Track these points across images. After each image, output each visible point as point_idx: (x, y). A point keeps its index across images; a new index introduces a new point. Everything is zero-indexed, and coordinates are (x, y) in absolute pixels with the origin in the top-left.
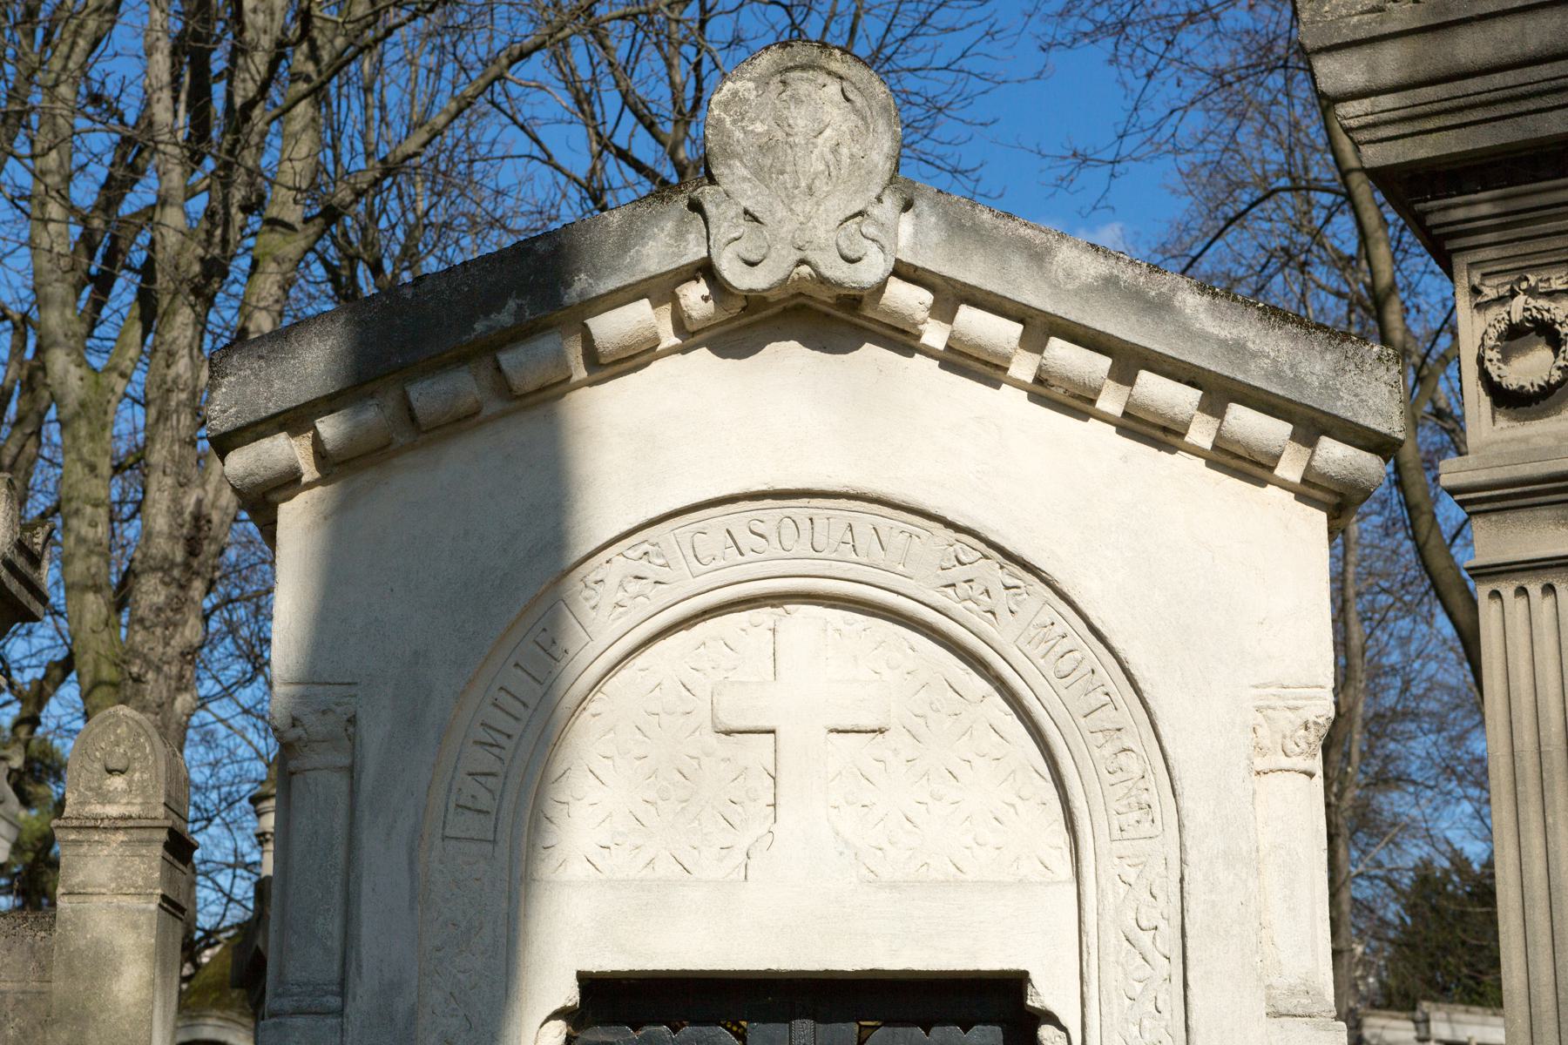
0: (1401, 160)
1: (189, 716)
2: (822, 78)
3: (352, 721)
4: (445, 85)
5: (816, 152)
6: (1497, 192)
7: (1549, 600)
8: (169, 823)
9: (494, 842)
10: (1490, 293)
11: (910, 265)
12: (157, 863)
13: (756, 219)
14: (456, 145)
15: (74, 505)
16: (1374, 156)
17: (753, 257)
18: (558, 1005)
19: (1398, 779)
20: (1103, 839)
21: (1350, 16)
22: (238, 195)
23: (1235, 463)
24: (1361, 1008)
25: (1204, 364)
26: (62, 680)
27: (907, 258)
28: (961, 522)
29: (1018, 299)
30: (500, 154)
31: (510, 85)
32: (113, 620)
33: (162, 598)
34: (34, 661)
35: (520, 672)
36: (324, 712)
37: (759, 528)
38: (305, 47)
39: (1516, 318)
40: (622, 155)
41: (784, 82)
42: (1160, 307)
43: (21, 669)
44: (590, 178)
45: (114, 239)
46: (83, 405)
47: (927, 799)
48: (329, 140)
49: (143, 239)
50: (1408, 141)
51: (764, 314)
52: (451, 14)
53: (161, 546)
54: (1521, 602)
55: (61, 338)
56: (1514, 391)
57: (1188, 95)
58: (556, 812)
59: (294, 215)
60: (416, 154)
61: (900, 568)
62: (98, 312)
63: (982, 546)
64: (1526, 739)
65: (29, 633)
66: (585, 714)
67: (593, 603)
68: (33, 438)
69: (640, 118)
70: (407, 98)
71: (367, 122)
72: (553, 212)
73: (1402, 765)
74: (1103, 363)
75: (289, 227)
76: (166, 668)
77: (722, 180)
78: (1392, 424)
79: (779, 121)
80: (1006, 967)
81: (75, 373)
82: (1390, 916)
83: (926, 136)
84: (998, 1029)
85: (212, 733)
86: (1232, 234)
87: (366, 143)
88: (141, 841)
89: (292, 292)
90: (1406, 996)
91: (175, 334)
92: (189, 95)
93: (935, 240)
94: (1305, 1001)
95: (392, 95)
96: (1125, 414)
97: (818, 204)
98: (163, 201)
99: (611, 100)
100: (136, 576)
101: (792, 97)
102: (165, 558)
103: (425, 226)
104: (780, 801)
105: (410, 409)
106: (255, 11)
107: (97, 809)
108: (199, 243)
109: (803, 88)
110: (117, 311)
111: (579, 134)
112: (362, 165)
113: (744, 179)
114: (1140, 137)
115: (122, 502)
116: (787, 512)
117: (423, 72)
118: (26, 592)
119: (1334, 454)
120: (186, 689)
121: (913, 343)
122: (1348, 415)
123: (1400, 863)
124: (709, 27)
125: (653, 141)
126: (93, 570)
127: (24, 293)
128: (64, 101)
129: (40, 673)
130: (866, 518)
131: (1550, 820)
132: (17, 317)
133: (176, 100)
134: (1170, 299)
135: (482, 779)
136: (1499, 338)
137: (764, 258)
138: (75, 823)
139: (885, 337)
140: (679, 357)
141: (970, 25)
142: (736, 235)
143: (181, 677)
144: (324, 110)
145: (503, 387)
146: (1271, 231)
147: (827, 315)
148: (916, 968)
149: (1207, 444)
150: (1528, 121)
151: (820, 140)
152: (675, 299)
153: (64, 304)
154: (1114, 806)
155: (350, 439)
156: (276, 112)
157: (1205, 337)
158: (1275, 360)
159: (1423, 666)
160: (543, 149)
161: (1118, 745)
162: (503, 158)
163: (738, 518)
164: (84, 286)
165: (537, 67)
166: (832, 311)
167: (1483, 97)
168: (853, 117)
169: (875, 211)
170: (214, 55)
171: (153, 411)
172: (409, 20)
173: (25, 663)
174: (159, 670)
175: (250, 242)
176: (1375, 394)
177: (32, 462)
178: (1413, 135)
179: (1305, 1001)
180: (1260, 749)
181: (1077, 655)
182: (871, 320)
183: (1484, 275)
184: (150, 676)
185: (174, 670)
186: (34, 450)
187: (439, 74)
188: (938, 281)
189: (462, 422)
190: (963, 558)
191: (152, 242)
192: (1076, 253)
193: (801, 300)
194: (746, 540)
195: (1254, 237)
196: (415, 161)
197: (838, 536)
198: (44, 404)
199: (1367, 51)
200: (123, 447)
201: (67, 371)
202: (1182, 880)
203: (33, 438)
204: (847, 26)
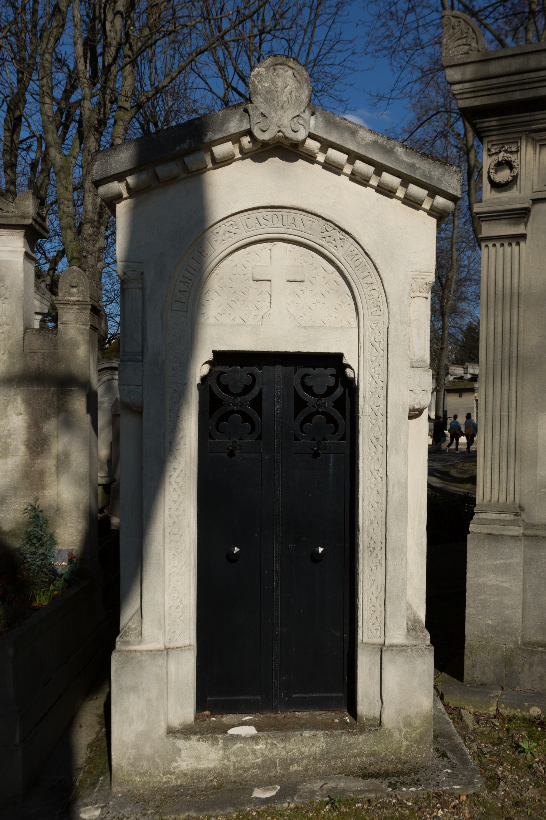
0: (470, 106)
1: (102, 269)
2: (287, 68)
3: (142, 274)
4: (176, 61)
5: (285, 94)
6: (498, 118)
7: (502, 248)
8: (91, 303)
9: (187, 312)
10: (493, 151)
11: (313, 134)
12: (88, 315)
13: (265, 116)
14: (180, 83)
15: (61, 200)
16: (463, 104)
17: (264, 129)
18: (207, 360)
19: (464, 298)
20: (366, 315)
21: (457, 55)
22: (108, 98)
23: (411, 203)
24: (449, 364)
25: (402, 171)
26: (63, 256)
27: (312, 131)
28: (328, 218)
29: (347, 147)
30: (195, 87)
31: (198, 64)
32: (76, 238)
33: (92, 231)
34: (53, 250)
35: (193, 260)
36: (133, 271)
37: (266, 217)
38: (128, 45)
39: (500, 159)
40: (235, 89)
41: (274, 69)
42: (390, 152)
43: (49, 253)
44: (224, 97)
45: (69, 111)
46: (62, 167)
47: (315, 302)
48: (138, 79)
49: (78, 112)
50: (473, 99)
51: (268, 148)
52: (177, 37)
53: (90, 215)
54: (494, 248)
55: (53, 144)
56: (497, 183)
57: (415, 78)
58: (206, 303)
59: (127, 105)
60: (166, 86)
61: (309, 232)
62: (65, 136)
63: (333, 226)
64: (492, 289)
65: (51, 241)
66: (214, 274)
67: (215, 239)
68: (47, 177)
69: (240, 77)
70: (164, 66)
71: (151, 74)
72: (212, 108)
73: (466, 295)
74: (372, 169)
75: (126, 109)
76: (94, 254)
77: (254, 102)
78: (457, 192)
79: (273, 83)
80: (337, 352)
81: (58, 156)
82: (460, 338)
83: (332, 88)
84: (334, 369)
85: (111, 274)
86: (426, 126)
87: (151, 81)
88: (83, 308)
89: (128, 132)
90: (462, 361)
91: (90, 144)
92: (90, 61)
93: (321, 126)
94: (421, 363)
95: (159, 64)
96: (378, 186)
97: (285, 112)
98: (84, 99)
99: (230, 70)
100: (83, 224)
101: (277, 74)
102: (92, 219)
103: (171, 111)
104: (272, 302)
105: (156, 175)
106: (110, 31)
107: (69, 298)
108: (96, 114)
109: (281, 72)
110: (71, 135)
111: (220, 81)
112: (150, 89)
113: (262, 102)
114: (398, 92)
115: (78, 200)
116: (275, 213)
117: (169, 57)
118: (41, 229)
119: (440, 201)
120: (101, 261)
121: (314, 160)
122: (445, 189)
123: (463, 323)
124: (263, 45)
125: (244, 86)
126: (69, 222)
127: (40, 128)
128: (47, 60)
129: (55, 254)
130: (299, 216)
131: (496, 313)
132: (38, 136)
133: (86, 62)
134: (393, 149)
135: (183, 293)
136: (495, 166)
137: (268, 129)
138: (62, 302)
139: (305, 157)
140: (241, 161)
141: (347, 50)
142: (259, 121)
143: (99, 257)
144: (136, 68)
145: (186, 169)
146: (438, 126)
147: (288, 149)
148: (311, 351)
149: (402, 196)
150: (510, 94)
151: (286, 90)
152: (240, 142)
153: (53, 132)
154: (370, 306)
155: (137, 184)
156: (119, 68)
157: (403, 162)
158: (424, 171)
159: (474, 265)
160: (209, 86)
161: (372, 288)
162: (196, 89)
163: (260, 214)
164: (60, 127)
165: (203, 58)
166: (289, 148)
167: (497, 85)
168: (296, 82)
169: (303, 115)
170: (98, 47)
171: (85, 170)
172: (162, 38)
173: (50, 250)
174: (92, 254)
175: (114, 114)
176: (453, 183)
177: (48, 185)
178: (474, 97)
179: (421, 363)
180: (413, 290)
181: (361, 260)
182: (301, 152)
183: (492, 145)
184: (89, 256)
185: (97, 255)
186: (48, 181)
187: (174, 57)
188: (322, 140)
189: (173, 180)
190: (328, 229)
191: (81, 113)
192: (365, 132)
193: (280, 144)
194: (262, 221)
195: (433, 127)
196: (166, 89)
197: (290, 221)
198: (50, 166)
199: (462, 68)
200: (77, 182)
201: (56, 156)
202: (388, 328)
203: (47, 177)
204: (307, 47)
